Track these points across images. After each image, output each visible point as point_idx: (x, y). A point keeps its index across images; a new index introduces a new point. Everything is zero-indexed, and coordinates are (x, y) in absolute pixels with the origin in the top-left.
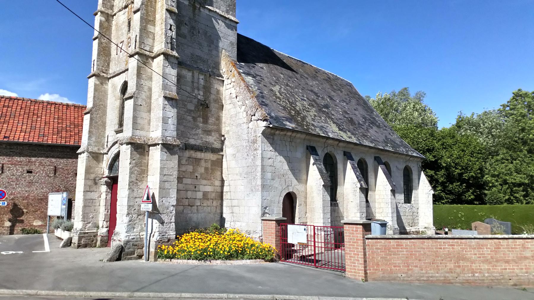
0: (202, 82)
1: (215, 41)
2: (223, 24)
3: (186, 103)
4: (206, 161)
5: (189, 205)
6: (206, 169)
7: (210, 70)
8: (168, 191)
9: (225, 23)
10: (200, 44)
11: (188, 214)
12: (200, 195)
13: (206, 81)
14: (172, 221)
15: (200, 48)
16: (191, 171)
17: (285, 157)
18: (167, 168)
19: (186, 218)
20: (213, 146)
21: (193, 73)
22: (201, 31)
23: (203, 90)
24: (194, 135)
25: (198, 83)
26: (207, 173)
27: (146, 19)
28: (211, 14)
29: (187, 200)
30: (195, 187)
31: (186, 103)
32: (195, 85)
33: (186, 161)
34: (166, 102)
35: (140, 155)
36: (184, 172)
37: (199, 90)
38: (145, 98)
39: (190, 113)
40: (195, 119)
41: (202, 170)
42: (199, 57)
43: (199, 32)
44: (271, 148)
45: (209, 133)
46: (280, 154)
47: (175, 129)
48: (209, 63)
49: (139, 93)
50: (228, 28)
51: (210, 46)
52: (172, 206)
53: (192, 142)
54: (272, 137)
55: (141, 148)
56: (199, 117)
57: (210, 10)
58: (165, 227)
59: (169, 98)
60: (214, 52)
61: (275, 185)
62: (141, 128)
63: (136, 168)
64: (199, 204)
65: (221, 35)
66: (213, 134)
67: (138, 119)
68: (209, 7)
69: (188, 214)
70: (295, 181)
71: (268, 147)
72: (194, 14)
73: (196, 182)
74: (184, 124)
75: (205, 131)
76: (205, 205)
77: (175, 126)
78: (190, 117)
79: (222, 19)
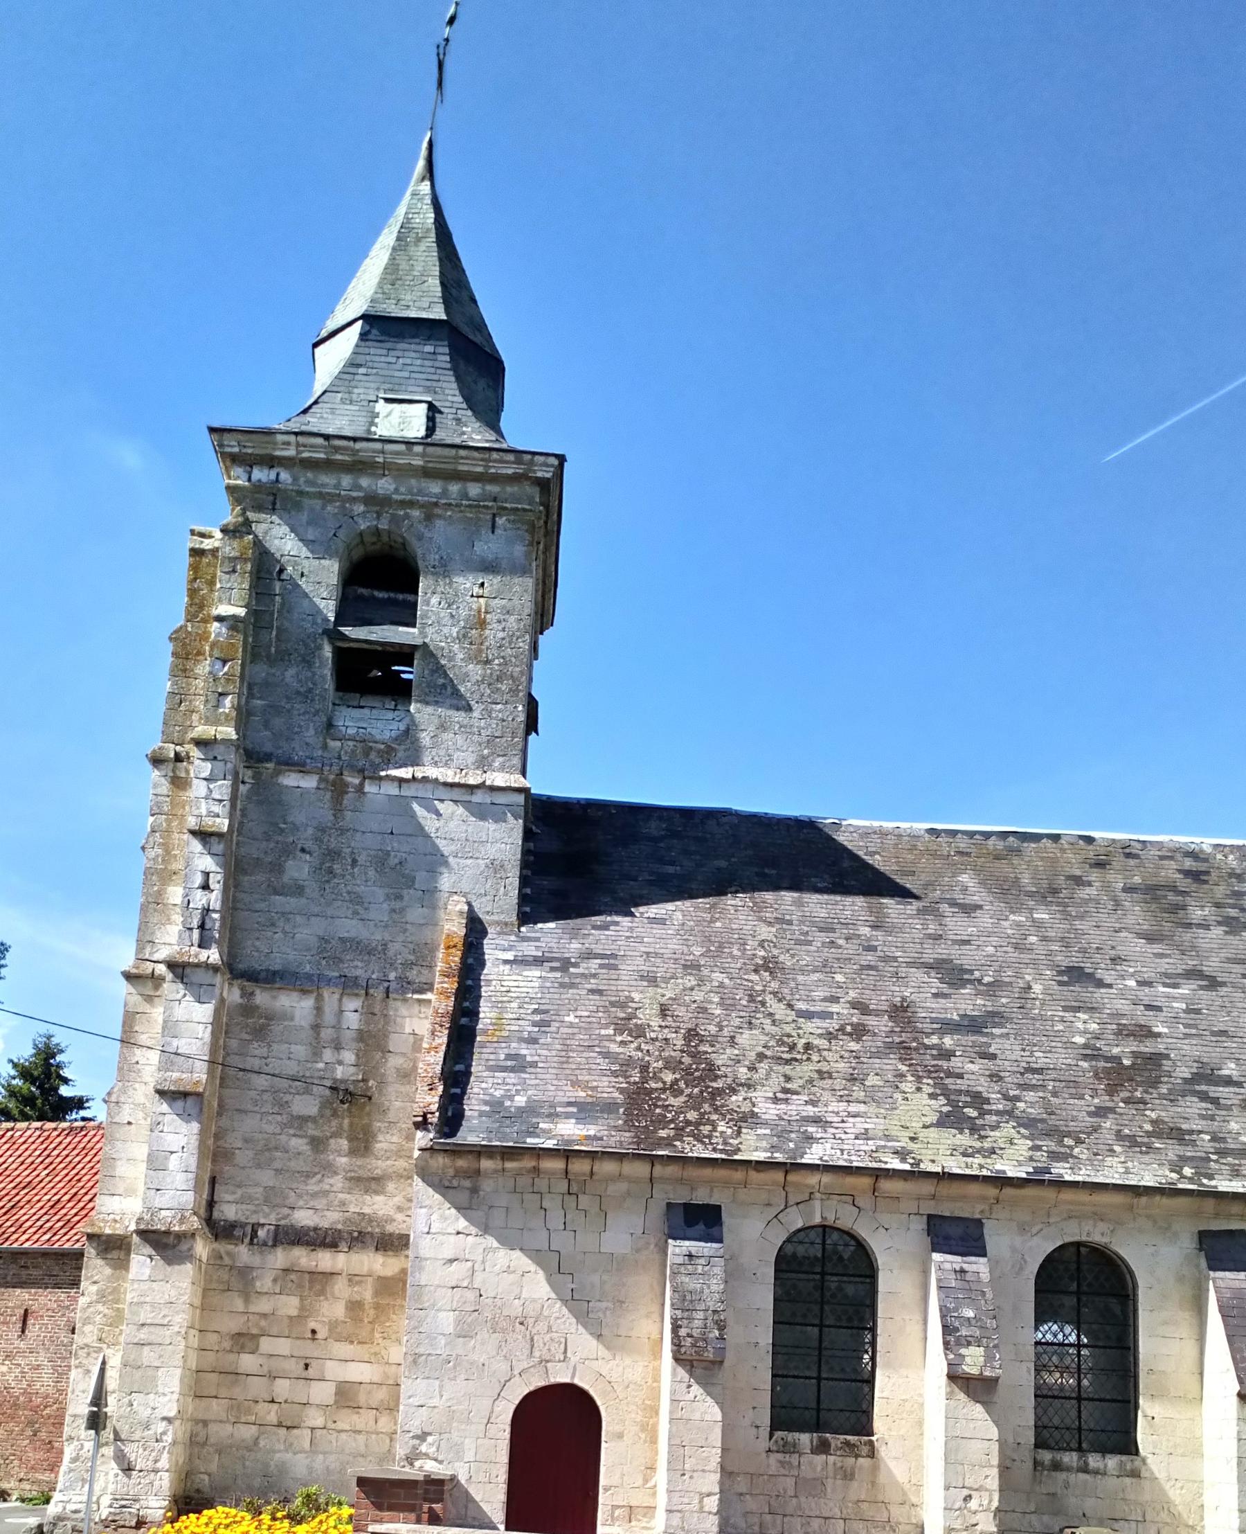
0: (352, 1020)
1: (421, 876)
2: (460, 810)
3: (288, 1097)
4: (353, 1279)
5: (280, 1425)
6: (355, 1307)
7: (392, 976)
8: (150, 1372)
9: (467, 805)
10: (357, 899)
11: (274, 1452)
12: (323, 1393)
13: (369, 1013)
14: (159, 1465)
15: (356, 913)
16: (294, 1312)
17: (536, 1255)
18: (152, 1305)
19: (267, 1465)
20: (390, 1228)
21: (319, 998)
22: (362, 859)
23: (354, 1045)
24: (314, 1195)
25: (337, 1027)
26: (357, 1320)
27: (159, 873)
28: (408, 791)
29: (276, 1406)
30: (307, 1366)
31: (288, 1097)
32: (327, 1034)
33: (275, 1280)
34: (165, 1107)
35: (115, 1268)
36: (265, 1316)
37: (338, 1047)
38: (142, 1100)
39: (300, 1128)
40: (318, 1144)
41: (333, 1309)
42: (351, 940)
43: (354, 862)
44: (462, 1224)
45: (373, 1185)
46: (507, 1242)
47: (191, 1184)
48: (391, 953)
49: (124, 1091)
50: (482, 817)
51: (399, 897)
52: (164, 1419)
53: (304, 1218)
54: (467, 1183)
55: (120, 1248)
56: (335, 1135)
57: (401, 781)
58: (133, 1484)
59: (174, 1092)
60: (415, 914)
61: (474, 1357)
62: (126, 1190)
63: (100, 1307)
64: (319, 1422)
65: (445, 847)
66: (391, 1186)
67: (119, 1163)
68: (394, 773)
69: (274, 1452)
70: (583, 1343)
71: (444, 1218)
72: (338, 810)
73: (308, 1349)
74: (277, 1165)
75: (359, 1179)
76: (340, 1426)
77: (191, 1176)
78: (300, 1141)
79: (457, 794)
